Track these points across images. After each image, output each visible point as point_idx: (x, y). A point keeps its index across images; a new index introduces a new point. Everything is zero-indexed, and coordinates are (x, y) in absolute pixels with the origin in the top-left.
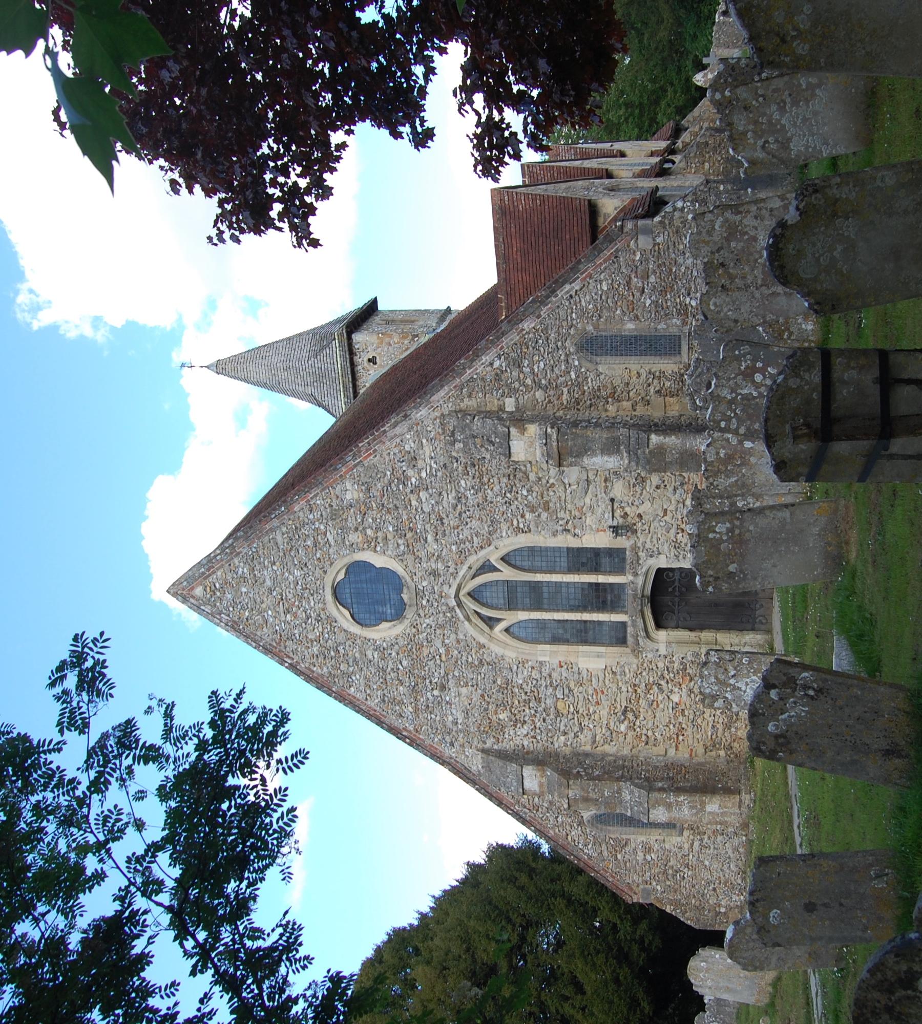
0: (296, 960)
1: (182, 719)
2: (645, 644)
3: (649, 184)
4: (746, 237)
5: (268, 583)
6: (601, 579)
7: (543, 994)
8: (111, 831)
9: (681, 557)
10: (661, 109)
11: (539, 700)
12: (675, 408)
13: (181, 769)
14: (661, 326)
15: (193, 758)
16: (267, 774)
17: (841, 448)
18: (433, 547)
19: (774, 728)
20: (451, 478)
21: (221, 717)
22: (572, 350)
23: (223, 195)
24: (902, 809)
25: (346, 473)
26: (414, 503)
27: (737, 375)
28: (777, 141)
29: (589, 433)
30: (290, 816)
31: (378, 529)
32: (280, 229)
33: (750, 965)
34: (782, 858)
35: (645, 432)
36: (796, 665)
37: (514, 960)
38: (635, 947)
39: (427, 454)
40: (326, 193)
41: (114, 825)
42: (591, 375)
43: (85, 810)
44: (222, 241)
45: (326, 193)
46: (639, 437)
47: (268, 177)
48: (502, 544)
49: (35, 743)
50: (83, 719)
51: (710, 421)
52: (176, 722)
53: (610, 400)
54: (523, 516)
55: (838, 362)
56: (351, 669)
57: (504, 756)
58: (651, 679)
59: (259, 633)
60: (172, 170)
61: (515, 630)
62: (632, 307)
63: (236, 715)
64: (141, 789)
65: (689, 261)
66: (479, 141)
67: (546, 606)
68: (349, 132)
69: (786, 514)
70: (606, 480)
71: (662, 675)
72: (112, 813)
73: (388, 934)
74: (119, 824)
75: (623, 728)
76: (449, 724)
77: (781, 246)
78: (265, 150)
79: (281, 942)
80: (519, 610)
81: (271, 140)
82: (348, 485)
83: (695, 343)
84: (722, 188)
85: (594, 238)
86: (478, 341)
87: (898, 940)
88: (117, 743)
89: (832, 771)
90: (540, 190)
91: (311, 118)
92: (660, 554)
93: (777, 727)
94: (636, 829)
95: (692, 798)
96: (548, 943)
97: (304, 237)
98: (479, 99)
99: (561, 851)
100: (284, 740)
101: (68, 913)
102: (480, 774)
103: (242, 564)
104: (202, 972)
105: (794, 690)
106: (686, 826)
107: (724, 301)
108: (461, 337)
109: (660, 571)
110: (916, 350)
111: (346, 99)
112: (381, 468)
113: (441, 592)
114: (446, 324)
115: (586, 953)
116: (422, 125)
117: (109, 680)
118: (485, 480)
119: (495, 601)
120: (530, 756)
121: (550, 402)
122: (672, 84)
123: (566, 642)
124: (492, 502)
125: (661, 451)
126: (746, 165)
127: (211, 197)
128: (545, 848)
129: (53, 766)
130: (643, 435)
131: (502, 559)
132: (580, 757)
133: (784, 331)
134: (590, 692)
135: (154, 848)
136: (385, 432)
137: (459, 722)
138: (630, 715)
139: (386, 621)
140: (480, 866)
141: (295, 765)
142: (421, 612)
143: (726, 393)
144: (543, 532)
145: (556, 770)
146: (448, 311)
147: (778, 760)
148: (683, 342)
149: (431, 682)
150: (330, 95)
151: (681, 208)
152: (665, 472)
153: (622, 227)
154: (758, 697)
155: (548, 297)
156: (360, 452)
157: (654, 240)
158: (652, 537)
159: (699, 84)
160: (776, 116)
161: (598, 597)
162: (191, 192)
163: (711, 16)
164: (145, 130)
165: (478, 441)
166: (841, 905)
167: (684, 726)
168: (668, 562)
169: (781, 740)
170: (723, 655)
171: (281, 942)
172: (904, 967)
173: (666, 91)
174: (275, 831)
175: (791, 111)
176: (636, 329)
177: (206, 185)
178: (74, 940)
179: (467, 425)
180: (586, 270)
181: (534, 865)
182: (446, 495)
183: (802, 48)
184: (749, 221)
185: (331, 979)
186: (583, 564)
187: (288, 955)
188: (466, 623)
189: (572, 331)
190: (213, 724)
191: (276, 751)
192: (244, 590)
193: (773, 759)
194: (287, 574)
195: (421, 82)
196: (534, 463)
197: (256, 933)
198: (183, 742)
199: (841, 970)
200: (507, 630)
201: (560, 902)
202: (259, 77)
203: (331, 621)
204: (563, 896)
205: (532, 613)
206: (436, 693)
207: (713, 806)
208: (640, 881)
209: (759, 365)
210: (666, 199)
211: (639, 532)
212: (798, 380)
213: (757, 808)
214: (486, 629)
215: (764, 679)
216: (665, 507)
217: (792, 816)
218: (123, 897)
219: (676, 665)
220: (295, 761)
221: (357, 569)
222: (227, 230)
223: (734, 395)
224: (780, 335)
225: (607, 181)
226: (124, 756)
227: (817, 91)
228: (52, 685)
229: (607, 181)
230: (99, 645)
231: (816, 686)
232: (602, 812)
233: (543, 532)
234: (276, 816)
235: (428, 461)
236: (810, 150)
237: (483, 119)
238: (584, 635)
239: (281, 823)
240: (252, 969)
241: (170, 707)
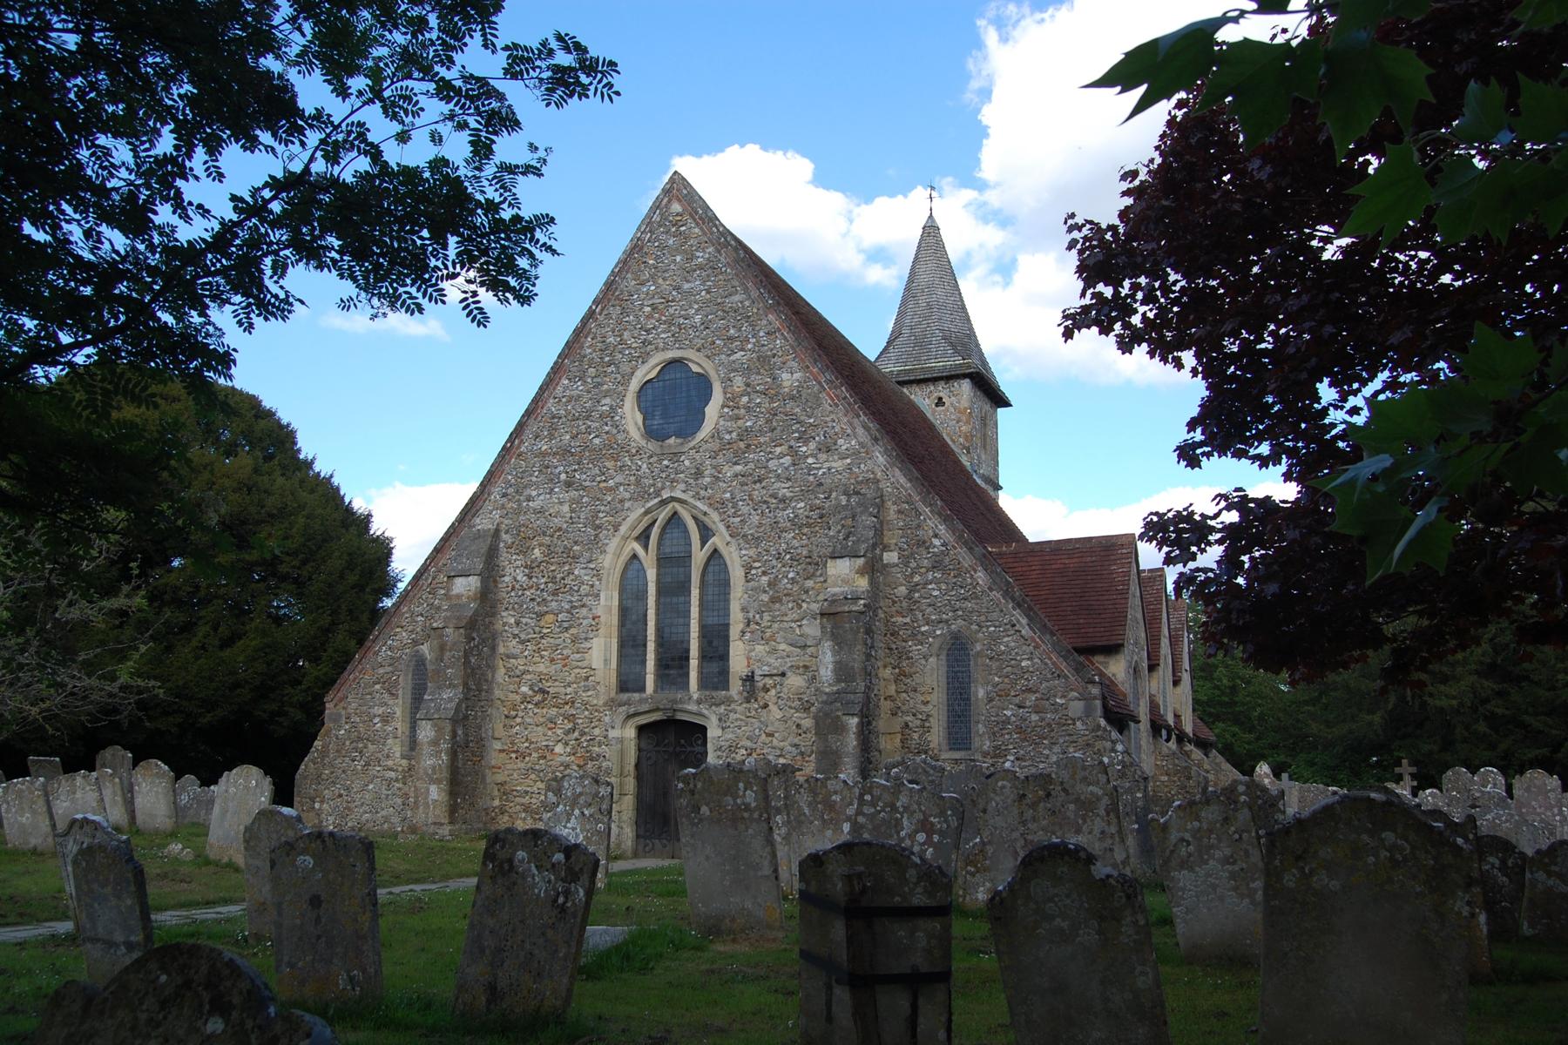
1: (524, 186)
5: (686, 286)
6: (694, 663)
8: (394, 105)
10: (1227, 723)
11: (555, 593)
12: (889, 745)
14: (981, 728)
15: (478, 196)
16: (460, 280)
17: (839, 930)
18: (729, 471)
21: (525, 228)
24: (428, 1006)
26: (778, 450)
28: (1190, 855)
31: (748, 409)
32: (1083, 295)
33: (251, 836)
34: (373, 868)
38: (274, 707)
40: (1125, 346)
41: (401, 107)
43: (416, 75)
44: (1070, 230)
45: (1125, 346)
46: (855, 705)
47: (1143, 280)
49: (494, 19)
50: (521, 72)
52: (520, 178)
54: (764, 573)
55: (936, 925)
57: (492, 554)
60: (1149, 172)
61: (636, 564)
62: (1003, 694)
65: (1054, 759)
66: (1185, 517)
68: (1194, 372)
69: (767, 871)
70: (805, 667)
75: (524, 689)
76: (527, 492)
77: (1066, 858)
78: (1173, 277)
82: (797, 376)
83: (962, 767)
84: (1139, 795)
85: (1079, 651)
87: (267, 993)
89: (472, 926)
90: (1134, 589)
96: (279, 607)
97: (1074, 323)
98: (1232, 517)
101: (303, 60)
104: (235, 208)
108: (970, 504)
109: (703, 729)
110: (951, 1014)
112: (818, 412)
116: (1203, 454)
118: (805, 530)
119: (668, 542)
122: (1258, 739)
125: (840, 729)
128: (388, 603)
129: (467, 39)
130: (857, 709)
132: (491, 640)
135: (375, 153)
138: (538, 698)
140: (367, 529)
143: (903, 800)
146: (998, 488)
147: (484, 864)
151: (1115, 750)
153: (1093, 682)
154: (556, 839)
155: (1013, 599)
160: (1218, 854)
161: (673, 659)
162: (1124, 194)
163: (1335, 782)
164: (1193, 141)
166: (319, 937)
169: (506, 866)
170: (607, 801)
172: (236, 1000)
174: (396, 290)
178: (270, 63)
179: (867, 508)
183: (1290, 880)
184: (1098, 825)
185: (227, 354)
186: (710, 643)
189: (974, 627)
190: (517, 219)
192: (678, 258)
195: (1252, 452)
197: (280, 269)
199: (245, 939)
200: (635, 556)
201: (326, 620)
202: (1255, 270)
203: (644, 358)
204: (333, 623)
206: (563, 476)
207: (435, 793)
209: (936, 838)
213: (434, 843)
215: (577, 846)
218: (319, 118)
221: (703, 387)
228: (559, 38)
234: (413, 290)
235: (826, 465)
237: (1212, 523)
238: (630, 643)
240: (240, 265)
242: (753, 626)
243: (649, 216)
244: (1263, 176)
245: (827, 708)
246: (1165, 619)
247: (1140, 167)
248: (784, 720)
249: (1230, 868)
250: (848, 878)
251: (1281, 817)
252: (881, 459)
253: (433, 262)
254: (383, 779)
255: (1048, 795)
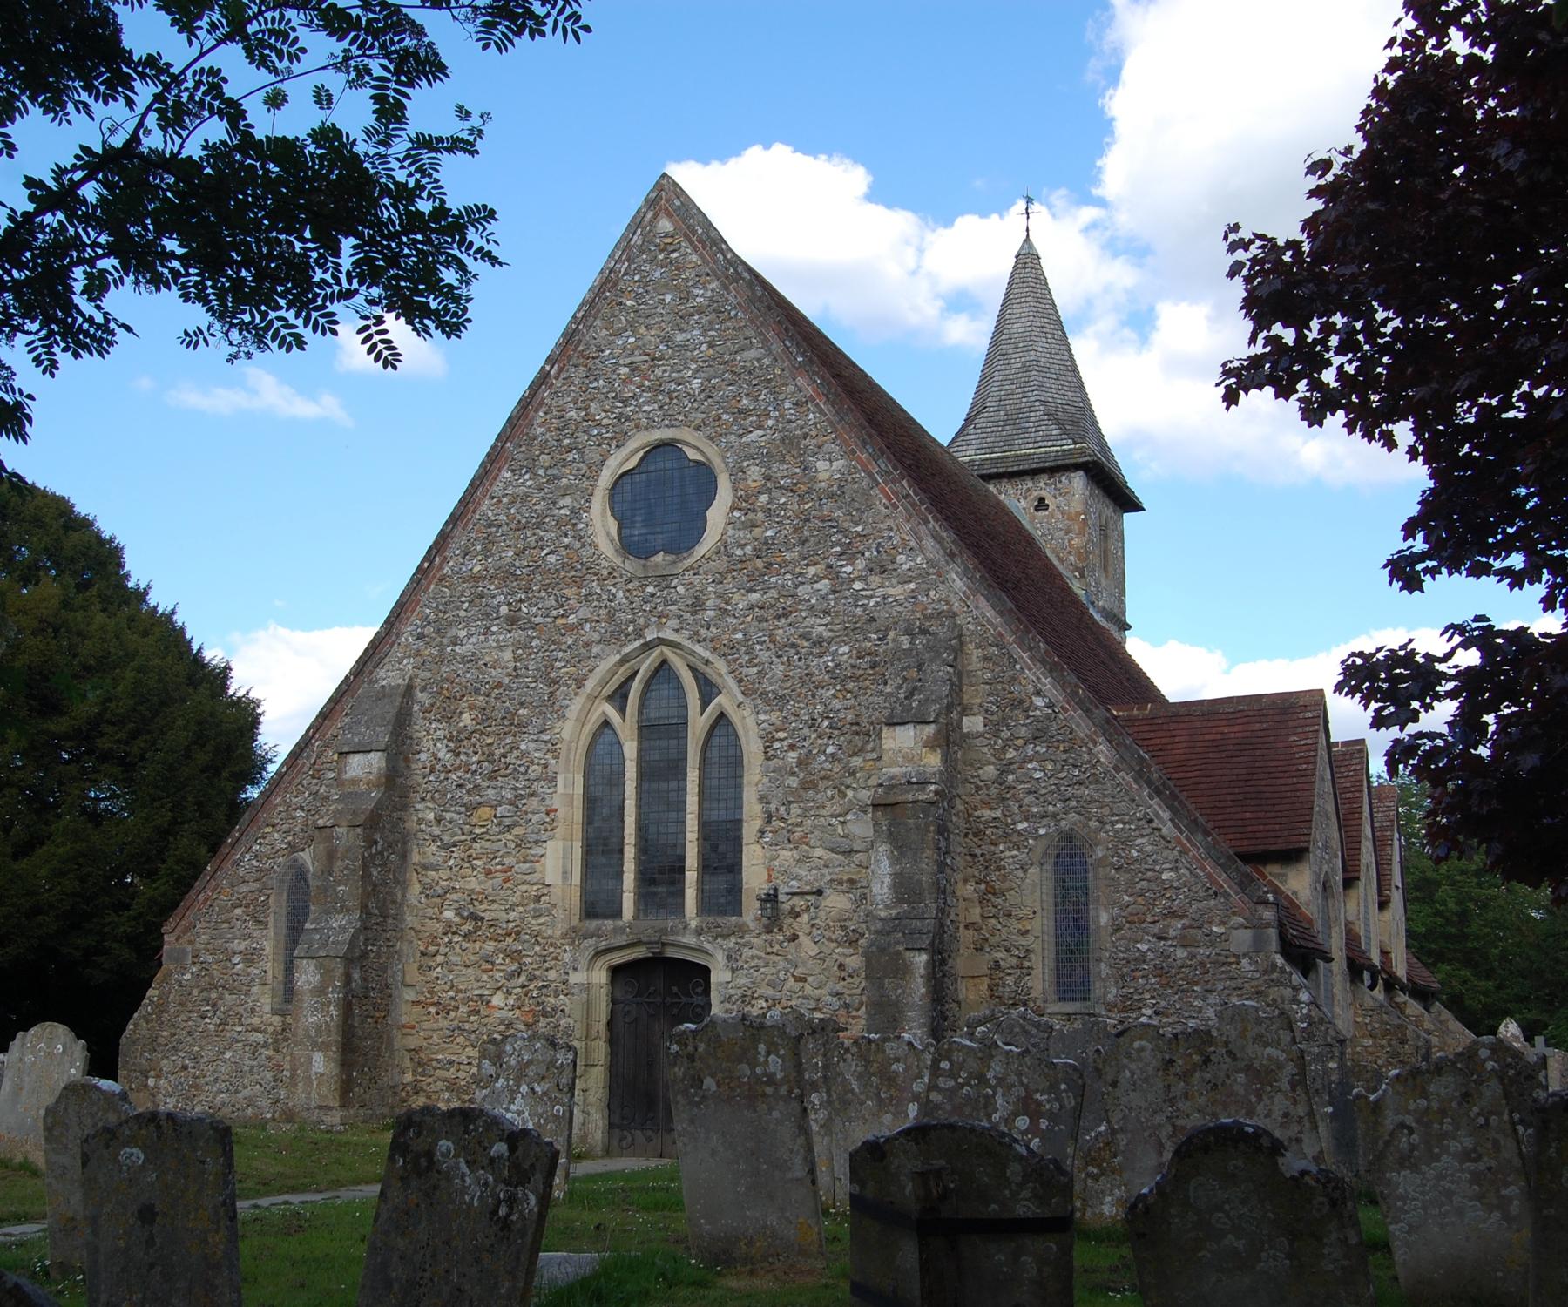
0: (50, 346)
2: (586, 949)
3: (1337, 946)
4: (1254, 1100)
5: (680, 337)
6: (691, 876)
7: (15, 791)
8: (262, 44)
9: (728, 1006)
11: (492, 777)
12: (971, 994)
13: (366, 165)
14: (1104, 969)
16: (359, 300)
17: (908, 1254)
18: (741, 602)
19: (444, 1149)
20: (852, 630)
21: (453, 226)
22: (1063, 823)
23: (1306, 249)
25: (859, 461)
26: (812, 570)
27: (1026, 1088)
28: (1413, 1148)
29: (928, 852)
30: (289, 339)
31: (768, 513)
32: (1253, 340)
33: (54, 1121)
35: (932, 944)
36: (549, 1185)
37: (69, 744)
39: (891, 591)
40: (1313, 415)
41: (272, 47)
42: (1022, 856)
44: (1232, 248)
45: (1313, 415)
46: (923, 935)
47: (1338, 320)
48: (745, 713)
51: (950, 1044)
52: (445, 157)
53: (983, 886)
54: (792, 747)
55: (1050, 1245)
56: (541, 472)
57: (402, 721)
58: (528, 960)
59: (598, 322)
62: (1136, 920)
63: (456, 252)
64: (335, 99)
66: (1403, 658)
67: (645, 786)
68: (1412, 453)
69: (799, 1171)
70: (852, 881)
71: (535, 978)
72: (292, 45)
73: (112, 539)
74: (274, 58)
76: (453, 632)
79: (80, 320)
80: (640, 742)
81: (1397, 323)
83: (1078, 1025)
84: (1333, 1065)
85: (1246, 858)
86: (1076, 671)
88: (406, 50)
90: (1323, 769)
91: (1434, 385)
92: (733, 971)
93: (446, 1155)
94: (283, 938)
95: (334, 1030)
96: (97, 799)
97: (1239, 380)
98: (1470, 658)
99: (246, 815)
100: (415, 329)
102: (372, 682)
103: (709, 294)
104: (32, 198)
105: (507, 1183)
106: (289, 1019)
107: (1147, 1064)
109: (705, 972)
111: (1466, 449)
113: (667, 616)
114: (1104, 623)
115: (81, 860)
116: (1426, 571)
117: (511, 42)
118: (851, 686)
120: (402, 764)
121: (978, 788)
122: (1500, 987)
123: (588, 820)
124: (813, 696)
125: (900, 970)
126: (1372, 1098)
127: (1303, 230)
128: (253, 792)
130: (926, 941)
131: (722, 715)
132: (401, 844)
133: (1099, 1166)
134: (506, 861)
135: (233, 112)
136: (926, 522)
137: (457, 648)
138: (469, 926)
139: (620, 528)
141: (374, 346)
142: (635, 584)
143: (995, 1069)
144: (766, 780)
145: (379, 805)
146: (1125, 627)
147: (391, 1158)
148: (1078, 1004)
149: (521, 601)
150: (1472, 420)
152: (866, 978)
153: (1266, 902)
154: (495, 1122)
155: (1149, 783)
156: (893, 482)
157: (1245, 955)
158: (759, 958)
159: (1502, 1028)
160: (1454, 1146)
161: (661, 871)
162: (1313, 193)
165: (914, 673)
166: (152, 1266)
167: (452, 1014)
168: (720, 984)
169: (423, 1162)
171: (80, 320)
173: (1488, 978)
174: (264, 315)
175: (1462, 1171)
176: (1098, 927)
177: (1323, 218)
179: (939, 654)
180: (1193, 845)
181: (225, 774)
182: (824, 621)
186: (715, 847)
187: (58, 333)
188: (618, 657)
189: (1094, 824)
191: (397, 318)
193: (392, 1149)
194: (693, 366)
195: (1497, 565)
196: (879, 764)
197: (97, 287)
198: (412, 169)
199: (46, 1271)
200: (606, 724)
203: (620, 440)
205: (634, 764)
206: (504, 610)
207: (321, 1063)
208: (198, 946)
209: (1044, 1123)
210: (1312, 976)
211: (769, 937)
212: (1019, 1179)
213: (318, 1136)
214: (608, 690)
215: (525, 1132)
216: (810, 979)
217: (303, 1192)
218: (153, 66)
219: (551, 1000)
220: (380, 346)
222: (1250, 255)
223: (993, 1082)
224: (1094, 1159)
225: (1339, 878)
226: (386, 62)
227: (1497, 1215)
229: (1339, 878)
230: (568, 25)
231: (514, 1218)
232: (311, 882)
233: (766, 780)
234: (290, 315)
235: (881, 592)
236: (1399, 1204)
237: (1441, 667)
238: (600, 848)
239: (278, 324)
241: (469, 148)
242: (776, 823)
243: (626, 240)
244: (1513, 165)
245: (883, 940)
246: (1366, 813)
247: (1334, 156)
248: (820, 958)
249: (1472, 1166)
250: (922, 1176)
251: (1542, 1095)
252: (959, 584)
253: (319, 275)
254: (246, 1043)
255: (1207, 1061)
